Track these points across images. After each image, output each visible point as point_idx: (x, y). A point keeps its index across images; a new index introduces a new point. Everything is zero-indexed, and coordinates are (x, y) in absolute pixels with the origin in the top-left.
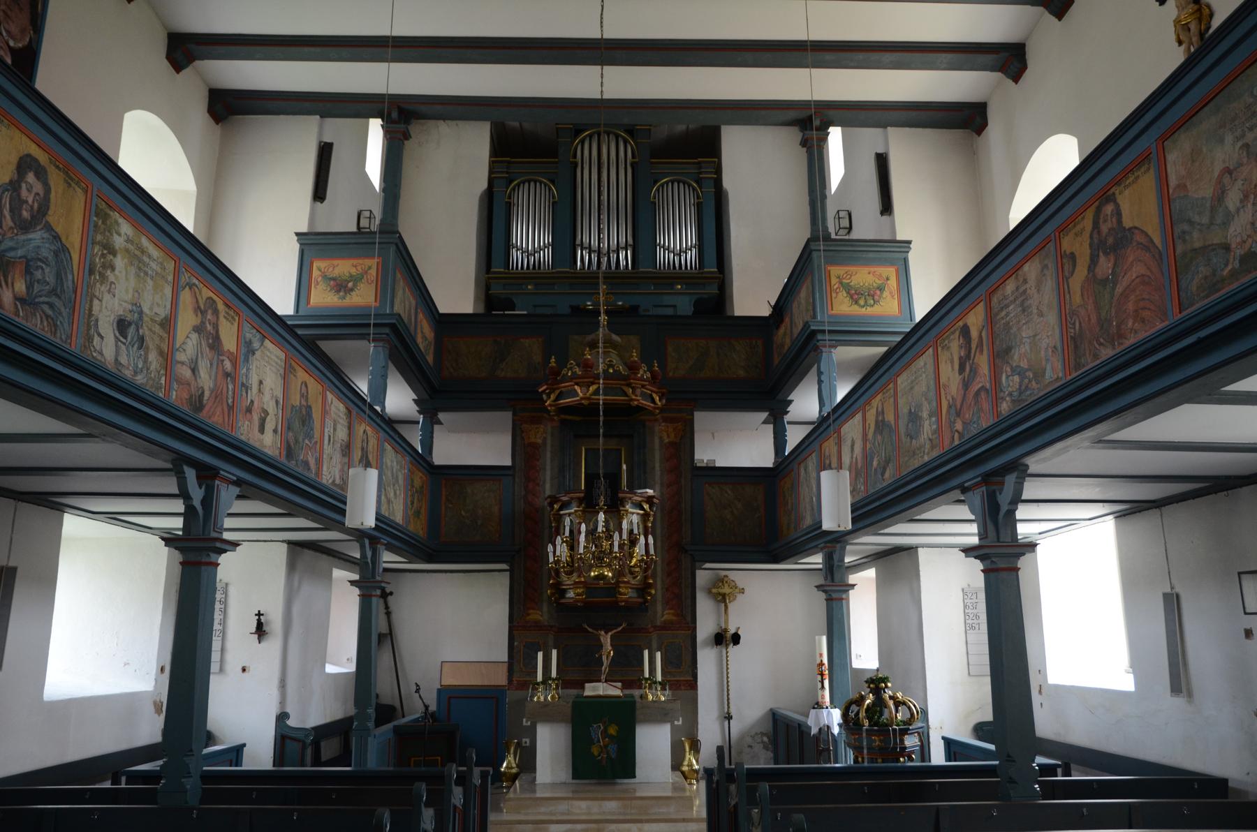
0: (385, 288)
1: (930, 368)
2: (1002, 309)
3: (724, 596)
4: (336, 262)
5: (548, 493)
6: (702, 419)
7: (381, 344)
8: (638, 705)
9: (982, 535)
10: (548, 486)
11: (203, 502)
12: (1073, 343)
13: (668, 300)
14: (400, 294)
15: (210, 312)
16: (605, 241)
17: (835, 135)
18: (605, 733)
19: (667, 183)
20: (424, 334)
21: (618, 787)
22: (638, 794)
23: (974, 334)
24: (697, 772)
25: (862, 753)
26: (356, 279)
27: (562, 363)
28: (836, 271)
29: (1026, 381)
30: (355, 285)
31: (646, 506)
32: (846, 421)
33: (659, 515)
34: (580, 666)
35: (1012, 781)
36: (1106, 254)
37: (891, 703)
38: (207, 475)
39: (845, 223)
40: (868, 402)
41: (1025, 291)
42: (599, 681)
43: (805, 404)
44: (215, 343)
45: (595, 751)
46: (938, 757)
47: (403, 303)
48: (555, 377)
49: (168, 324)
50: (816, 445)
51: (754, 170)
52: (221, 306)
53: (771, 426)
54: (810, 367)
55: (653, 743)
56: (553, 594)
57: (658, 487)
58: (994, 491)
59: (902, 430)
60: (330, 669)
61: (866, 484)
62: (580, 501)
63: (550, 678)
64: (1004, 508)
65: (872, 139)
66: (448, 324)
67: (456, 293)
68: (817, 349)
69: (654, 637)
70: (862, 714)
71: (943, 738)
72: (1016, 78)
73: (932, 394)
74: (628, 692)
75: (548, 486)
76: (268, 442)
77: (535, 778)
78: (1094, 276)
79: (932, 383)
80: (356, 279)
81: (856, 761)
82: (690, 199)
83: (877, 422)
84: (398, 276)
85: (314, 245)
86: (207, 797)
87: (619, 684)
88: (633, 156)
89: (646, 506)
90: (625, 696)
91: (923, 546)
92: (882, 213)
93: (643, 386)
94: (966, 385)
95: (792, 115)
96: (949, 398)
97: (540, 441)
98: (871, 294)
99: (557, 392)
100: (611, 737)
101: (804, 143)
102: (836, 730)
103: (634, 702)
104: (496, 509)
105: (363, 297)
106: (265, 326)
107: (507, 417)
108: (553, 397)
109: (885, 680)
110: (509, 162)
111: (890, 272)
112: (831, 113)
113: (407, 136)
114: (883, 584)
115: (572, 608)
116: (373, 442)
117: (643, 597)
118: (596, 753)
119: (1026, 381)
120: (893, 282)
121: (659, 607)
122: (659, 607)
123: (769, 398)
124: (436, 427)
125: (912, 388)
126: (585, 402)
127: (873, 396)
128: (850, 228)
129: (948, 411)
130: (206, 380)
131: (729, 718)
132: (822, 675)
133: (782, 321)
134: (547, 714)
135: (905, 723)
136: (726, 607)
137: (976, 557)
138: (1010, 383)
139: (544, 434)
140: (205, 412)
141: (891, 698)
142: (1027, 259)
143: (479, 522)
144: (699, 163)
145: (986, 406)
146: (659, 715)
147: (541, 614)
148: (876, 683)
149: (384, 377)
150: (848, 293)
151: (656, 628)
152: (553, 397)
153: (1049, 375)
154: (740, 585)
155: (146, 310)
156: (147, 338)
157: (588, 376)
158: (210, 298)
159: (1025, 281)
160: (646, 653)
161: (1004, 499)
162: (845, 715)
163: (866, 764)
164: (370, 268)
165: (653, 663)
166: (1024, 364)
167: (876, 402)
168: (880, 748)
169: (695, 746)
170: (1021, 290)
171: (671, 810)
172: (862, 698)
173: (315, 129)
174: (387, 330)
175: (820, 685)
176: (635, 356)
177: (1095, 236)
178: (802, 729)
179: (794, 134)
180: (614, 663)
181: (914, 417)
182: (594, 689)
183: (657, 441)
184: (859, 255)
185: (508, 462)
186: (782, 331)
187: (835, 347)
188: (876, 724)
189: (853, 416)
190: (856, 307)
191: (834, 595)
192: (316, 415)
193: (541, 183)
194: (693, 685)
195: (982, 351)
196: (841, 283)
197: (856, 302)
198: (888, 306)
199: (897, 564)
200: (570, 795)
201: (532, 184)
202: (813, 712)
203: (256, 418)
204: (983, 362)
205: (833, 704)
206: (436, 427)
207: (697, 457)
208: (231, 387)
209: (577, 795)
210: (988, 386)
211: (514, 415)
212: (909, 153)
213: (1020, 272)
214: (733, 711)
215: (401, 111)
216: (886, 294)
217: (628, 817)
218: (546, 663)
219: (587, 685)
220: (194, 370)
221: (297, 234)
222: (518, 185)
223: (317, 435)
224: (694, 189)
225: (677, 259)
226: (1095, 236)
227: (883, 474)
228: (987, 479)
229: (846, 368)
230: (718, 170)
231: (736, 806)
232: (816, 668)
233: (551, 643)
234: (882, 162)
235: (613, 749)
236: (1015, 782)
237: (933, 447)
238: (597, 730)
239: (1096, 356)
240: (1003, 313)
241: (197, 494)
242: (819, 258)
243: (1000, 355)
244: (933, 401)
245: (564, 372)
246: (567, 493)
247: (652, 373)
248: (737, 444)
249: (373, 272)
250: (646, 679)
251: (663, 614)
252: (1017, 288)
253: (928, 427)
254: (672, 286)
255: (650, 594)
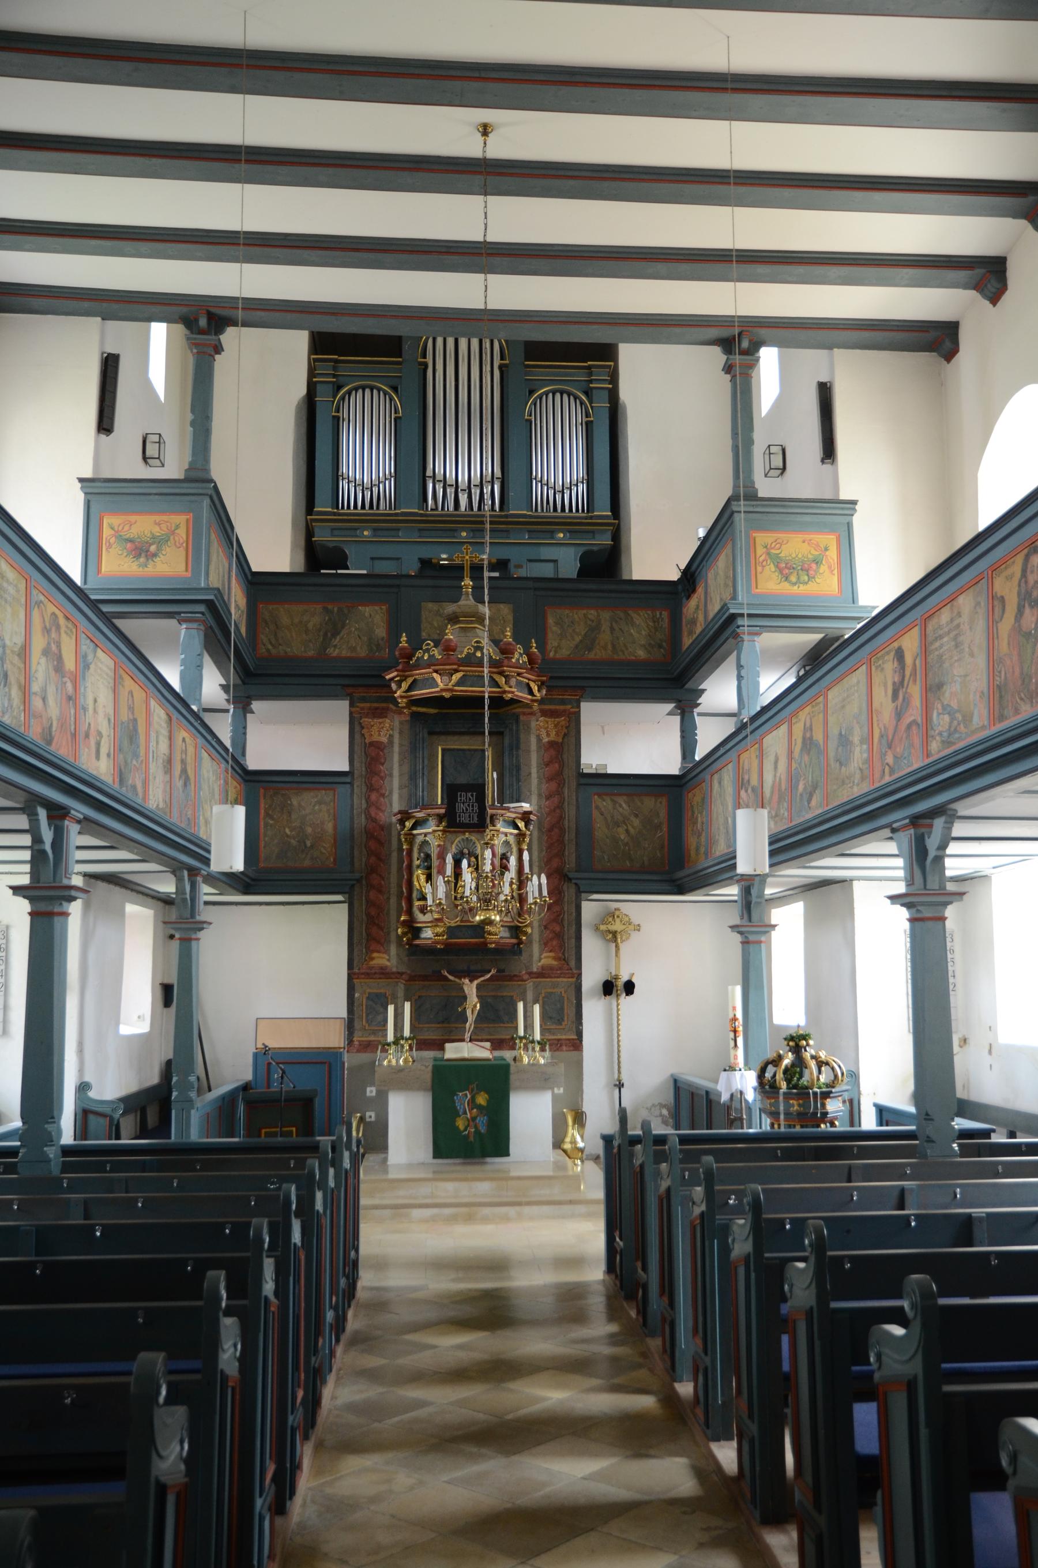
0: (196, 554)
1: (863, 688)
2: (936, 639)
3: (614, 934)
4: (132, 518)
5: (396, 808)
6: (591, 712)
7: (195, 625)
8: (512, 1069)
9: (910, 882)
10: (395, 797)
11: (54, 845)
12: (998, 694)
13: (546, 553)
14: (214, 558)
15: (53, 629)
16: (463, 465)
17: (769, 357)
18: (472, 1102)
19: (547, 394)
20: (237, 600)
21: (488, 1167)
22: (513, 1174)
23: (909, 660)
24: (582, 1150)
25: (778, 1119)
26: (161, 541)
27: (417, 643)
28: (762, 538)
29: (955, 723)
30: (159, 549)
31: (521, 825)
32: (769, 731)
33: (536, 834)
34: (439, 1022)
35: (929, 1140)
36: (1032, 607)
37: (813, 1064)
38: (58, 814)
39: (777, 461)
40: (795, 714)
41: (958, 626)
42: (463, 1040)
43: (719, 692)
44: (59, 667)
45: (460, 1124)
46: (869, 1122)
47: (218, 573)
48: (407, 661)
49: (24, 653)
50: (733, 754)
51: (664, 395)
52: (62, 621)
53: (678, 718)
54: (729, 653)
55: (530, 1114)
56: (404, 934)
57: (534, 798)
58: (923, 835)
59: (832, 754)
60: (125, 1030)
61: (790, 810)
62: (440, 818)
63: (402, 1038)
64: (932, 853)
65: (816, 363)
66: (262, 586)
67: (274, 551)
68: (736, 636)
69: (530, 985)
70: (780, 1076)
71: (876, 1105)
72: (994, 300)
73: (864, 717)
74: (498, 1053)
75: (395, 797)
76: (100, 767)
77: (385, 1160)
78: (1020, 626)
79: (864, 705)
80: (161, 541)
81: (772, 1125)
82: (577, 416)
83: (804, 738)
84: (213, 536)
85: (102, 493)
86: (66, 1168)
87: (488, 1045)
88: (502, 358)
89: (521, 825)
90: (495, 1058)
91: (859, 879)
92: (823, 461)
93: (519, 674)
94: (899, 715)
95: (714, 333)
96: (881, 725)
97: (385, 740)
98: (807, 568)
99: (410, 680)
100: (480, 1107)
101: (728, 369)
102: (750, 1096)
103: (508, 1066)
104: (329, 827)
105: (170, 566)
106: (98, 634)
107: (341, 707)
108: (405, 686)
109: (805, 1037)
110: (336, 361)
111: (830, 540)
112: (763, 332)
113: (218, 349)
114: (811, 921)
115: (429, 951)
116: (191, 750)
117: (517, 937)
118: (462, 1128)
119: (955, 723)
120: (833, 553)
121: (536, 948)
122: (536, 948)
123: (672, 679)
124: (248, 715)
125: (843, 707)
126: (447, 695)
127: (801, 708)
128: (784, 468)
129: (880, 741)
130: (54, 710)
131: (620, 1086)
132: (735, 1031)
133: (694, 591)
134: (401, 1080)
135: (827, 1085)
136: (617, 946)
137: (902, 905)
138: (941, 722)
139: (390, 731)
140: (54, 744)
141: (813, 1057)
142: (962, 591)
143: (308, 844)
144: (589, 367)
145: (917, 741)
146: (540, 1081)
147: (389, 958)
148: (796, 1042)
149: (200, 667)
150: (777, 567)
151: (531, 974)
152: (405, 686)
153: (976, 721)
154: (635, 920)
155: (8, 643)
156: (9, 673)
157: (450, 661)
158: (53, 614)
159: (959, 615)
160: (520, 1006)
161: (932, 843)
162: (761, 1076)
163: (782, 1129)
164: (178, 527)
165: (530, 1018)
166: (954, 704)
167: (803, 715)
168: (799, 1114)
169: (580, 1119)
170: (955, 623)
171: (556, 1192)
172: (780, 1058)
173: (96, 337)
174: (202, 608)
175: (732, 1043)
176: (508, 637)
177: (1023, 585)
178: (709, 1099)
179: (716, 355)
180: (481, 1018)
181: (844, 741)
182: (455, 1051)
183: (533, 740)
184: (792, 517)
185: (345, 767)
186: (693, 602)
187: (758, 634)
188: (795, 1087)
189: (777, 727)
190: (786, 585)
191: (751, 938)
192: (141, 729)
193: (379, 390)
194: (577, 1044)
195: (915, 681)
196: (768, 554)
197: (787, 579)
198: (826, 583)
199: (828, 897)
200: (430, 1176)
201: (368, 392)
202: (724, 1075)
203: (92, 741)
204: (915, 691)
205: (748, 1065)
206: (248, 715)
207: (584, 760)
208: (73, 712)
209: (438, 1176)
210: (919, 721)
211: (351, 705)
212: (862, 384)
213: (955, 603)
214: (625, 1079)
215: (211, 316)
216: (823, 568)
217: (505, 1200)
218: (399, 1018)
219: (448, 1046)
220: (44, 699)
221: (81, 480)
222: (349, 393)
223: (142, 752)
224: (581, 404)
225: (558, 497)
226: (1023, 585)
227: (809, 801)
228: (915, 821)
229: (772, 658)
230: (614, 377)
231: (642, 1166)
232: (728, 1024)
233: (401, 993)
234: (825, 395)
235: (482, 1122)
236: (933, 1142)
237: (863, 779)
238: (462, 1099)
239: (1017, 711)
240: (937, 644)
241: (48, 836)
242: (740, 521)
243: (932, 689)
244: (864, 727)
245: (418, 654)
246: (424, 807)
247: (530, 656)
248: (631, 742)
249: (182, 532)
250: (521, 1038)
251: (539, 957)
252: (952, 620)
253: (859, 754)
254: (552, 534)
255: (525, 933)
